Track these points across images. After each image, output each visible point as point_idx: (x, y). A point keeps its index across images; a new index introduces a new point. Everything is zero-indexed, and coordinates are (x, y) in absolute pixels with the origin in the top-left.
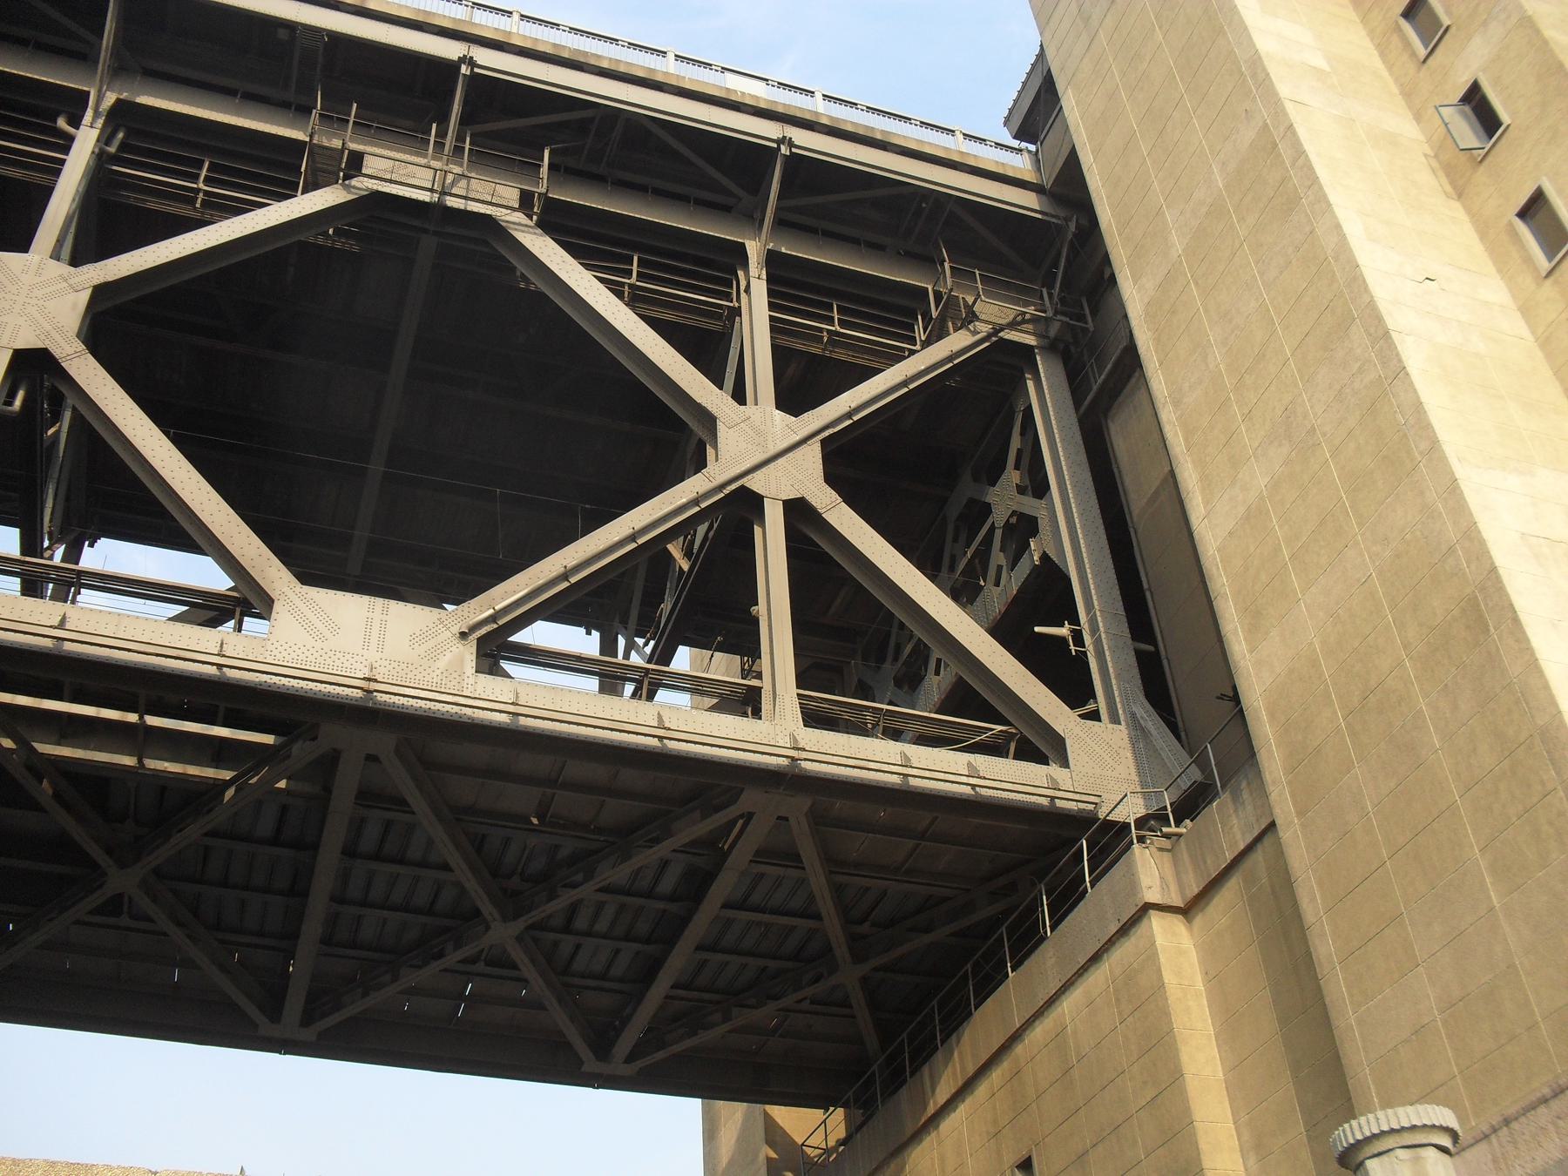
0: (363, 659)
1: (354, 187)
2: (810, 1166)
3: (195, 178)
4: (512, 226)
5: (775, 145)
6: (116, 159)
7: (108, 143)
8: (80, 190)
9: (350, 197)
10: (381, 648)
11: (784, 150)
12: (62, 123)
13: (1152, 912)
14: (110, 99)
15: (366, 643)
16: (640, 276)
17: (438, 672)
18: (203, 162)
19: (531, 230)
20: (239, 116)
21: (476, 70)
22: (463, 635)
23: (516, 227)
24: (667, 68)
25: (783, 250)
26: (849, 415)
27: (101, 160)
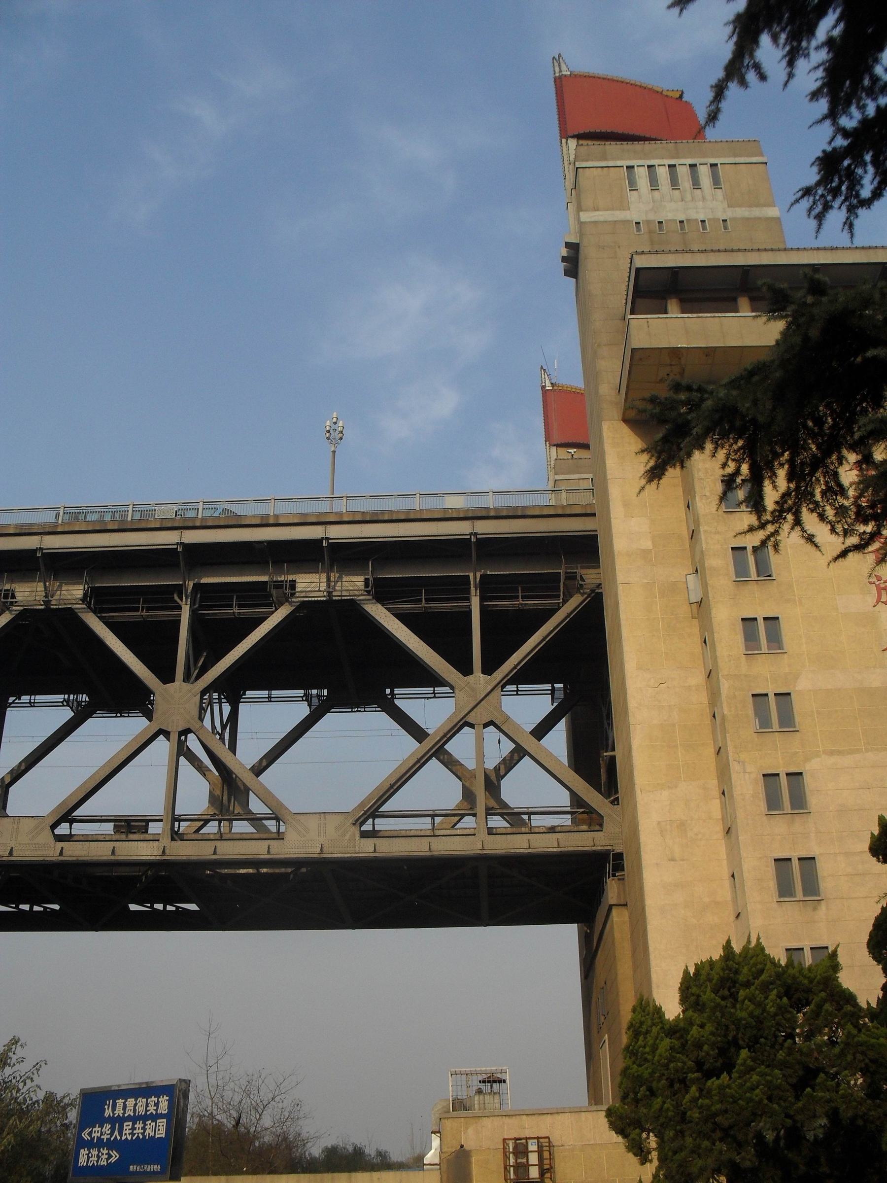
0: (318, 842)
1: (294, 602)
2: (260, 1111)
3: (231, 606)
4: (362, 602)
5: (469, 537)
6: (202, 607)
7: (194, 604)
8: (193, 857)
9: (293, 608)
10: (325, 835)
11: (473, 539)
12: (176, 598)
13: (613, 907)
14: (190, 585)
15: (319, 836)
16: (427, 600)
17: (346, 841)
18: (233, 596)
19: (371, 602)
20: (242, 576)
21: (330, 541)
22: (354, 824)
23: (364, 602)
24: (416, 504)
25: (488, 573)
26: (515, 668)
27: (194, 614)
